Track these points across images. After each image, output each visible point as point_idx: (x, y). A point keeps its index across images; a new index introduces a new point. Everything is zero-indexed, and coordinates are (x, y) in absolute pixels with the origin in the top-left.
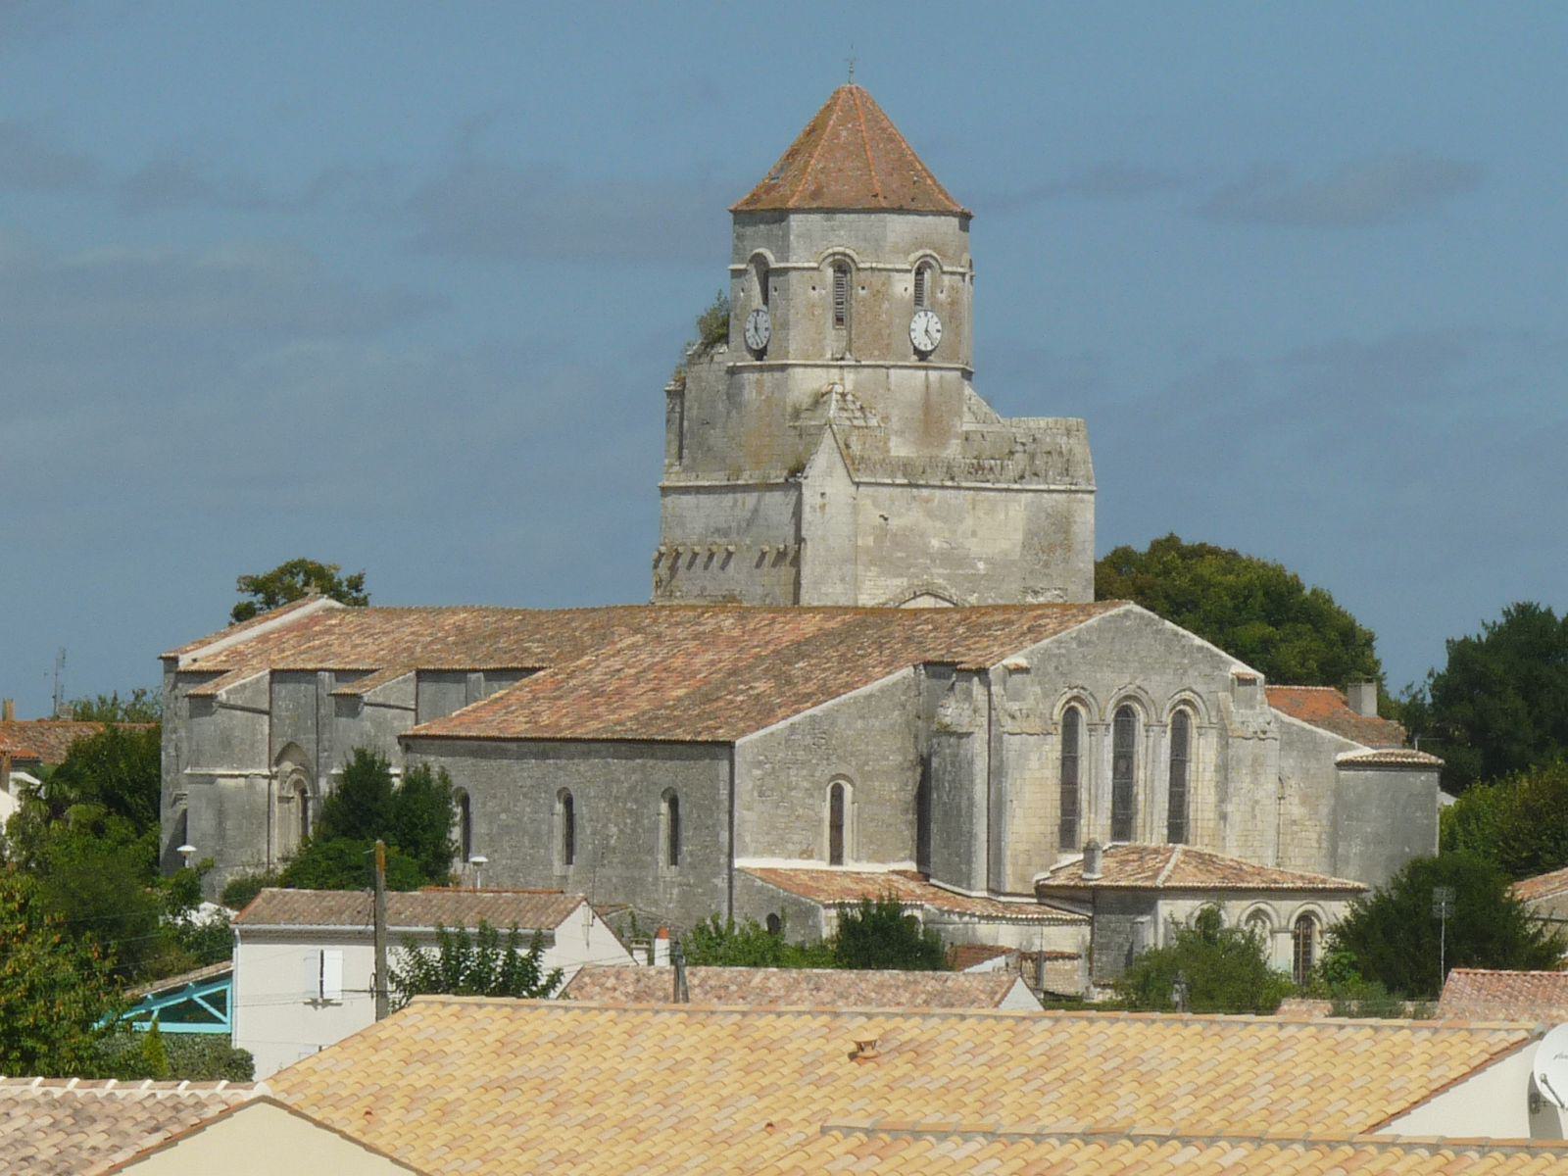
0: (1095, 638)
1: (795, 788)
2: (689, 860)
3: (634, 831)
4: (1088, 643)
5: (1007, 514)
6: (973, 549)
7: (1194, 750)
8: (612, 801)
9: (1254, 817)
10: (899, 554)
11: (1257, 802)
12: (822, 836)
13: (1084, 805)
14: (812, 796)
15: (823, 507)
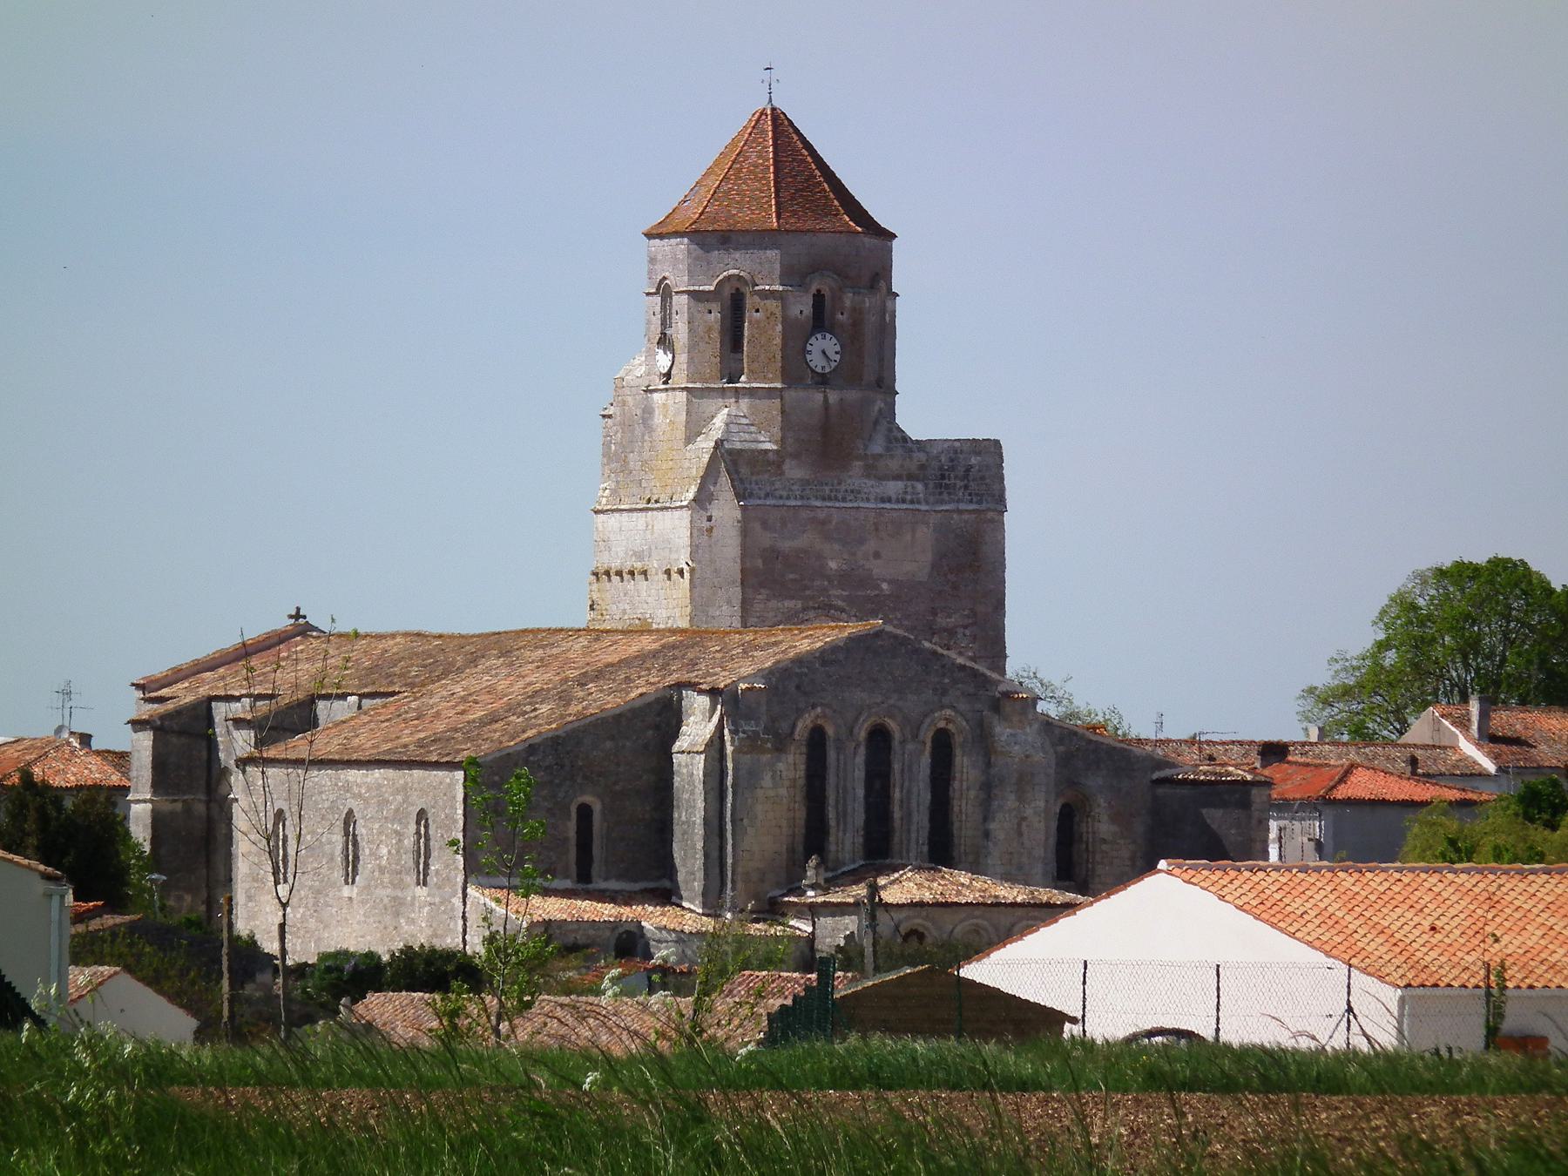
5: (913, 536)
9: (1020, 834)
10: (792, 576)
11: (1024, 819)
13: (832, 823)
15: (710, 530)
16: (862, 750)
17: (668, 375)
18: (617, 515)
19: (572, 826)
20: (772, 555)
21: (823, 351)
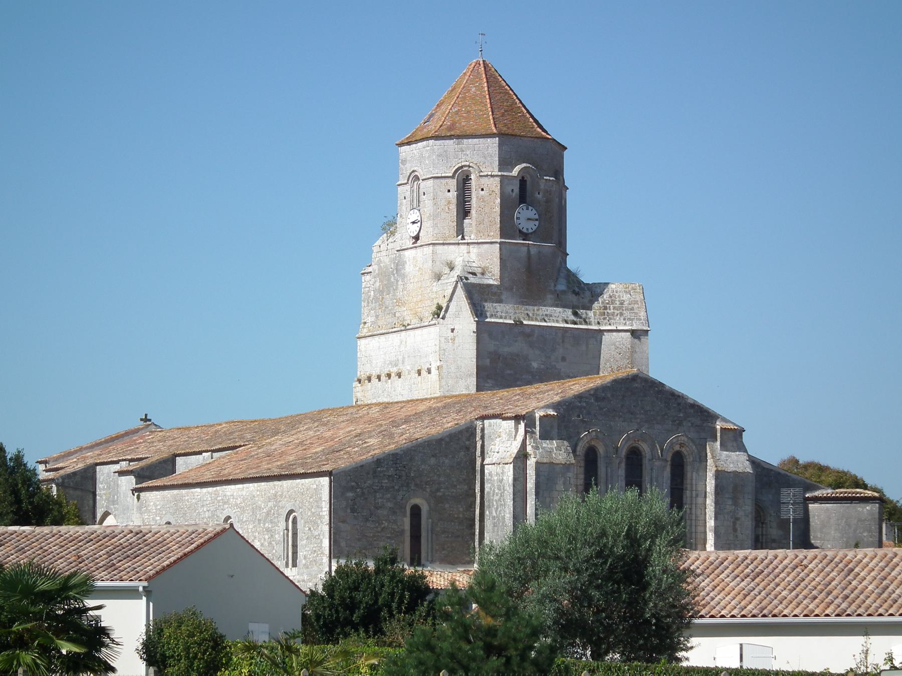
0: (609, 395)
1: (381, 507)
2: (304, 562)
3: (270, 543)
4: (604, 399)
5: (587, 347)
6: (563, 370)
7: (689, 481)
8: (257, 522)
9: (735, 530)
10: (509, 372)
11: (737, 519)
12: (403, 542)
14: (394, 513)
15: (453, 339)
16: (623, 465)
17: (417, 238)
18: (376, 338)
19: (407, 521)
20: (495, 357)
21: (526, 218)
